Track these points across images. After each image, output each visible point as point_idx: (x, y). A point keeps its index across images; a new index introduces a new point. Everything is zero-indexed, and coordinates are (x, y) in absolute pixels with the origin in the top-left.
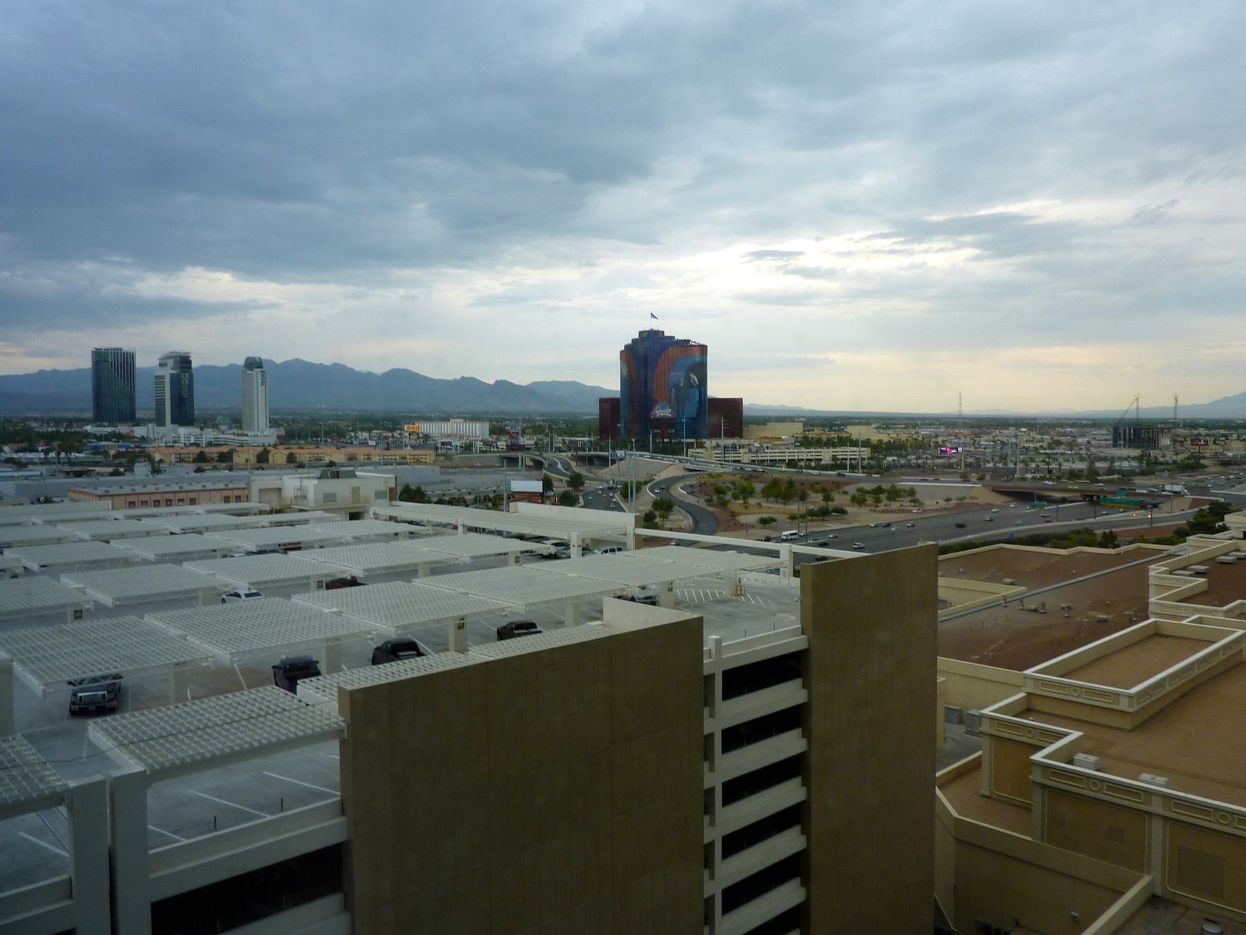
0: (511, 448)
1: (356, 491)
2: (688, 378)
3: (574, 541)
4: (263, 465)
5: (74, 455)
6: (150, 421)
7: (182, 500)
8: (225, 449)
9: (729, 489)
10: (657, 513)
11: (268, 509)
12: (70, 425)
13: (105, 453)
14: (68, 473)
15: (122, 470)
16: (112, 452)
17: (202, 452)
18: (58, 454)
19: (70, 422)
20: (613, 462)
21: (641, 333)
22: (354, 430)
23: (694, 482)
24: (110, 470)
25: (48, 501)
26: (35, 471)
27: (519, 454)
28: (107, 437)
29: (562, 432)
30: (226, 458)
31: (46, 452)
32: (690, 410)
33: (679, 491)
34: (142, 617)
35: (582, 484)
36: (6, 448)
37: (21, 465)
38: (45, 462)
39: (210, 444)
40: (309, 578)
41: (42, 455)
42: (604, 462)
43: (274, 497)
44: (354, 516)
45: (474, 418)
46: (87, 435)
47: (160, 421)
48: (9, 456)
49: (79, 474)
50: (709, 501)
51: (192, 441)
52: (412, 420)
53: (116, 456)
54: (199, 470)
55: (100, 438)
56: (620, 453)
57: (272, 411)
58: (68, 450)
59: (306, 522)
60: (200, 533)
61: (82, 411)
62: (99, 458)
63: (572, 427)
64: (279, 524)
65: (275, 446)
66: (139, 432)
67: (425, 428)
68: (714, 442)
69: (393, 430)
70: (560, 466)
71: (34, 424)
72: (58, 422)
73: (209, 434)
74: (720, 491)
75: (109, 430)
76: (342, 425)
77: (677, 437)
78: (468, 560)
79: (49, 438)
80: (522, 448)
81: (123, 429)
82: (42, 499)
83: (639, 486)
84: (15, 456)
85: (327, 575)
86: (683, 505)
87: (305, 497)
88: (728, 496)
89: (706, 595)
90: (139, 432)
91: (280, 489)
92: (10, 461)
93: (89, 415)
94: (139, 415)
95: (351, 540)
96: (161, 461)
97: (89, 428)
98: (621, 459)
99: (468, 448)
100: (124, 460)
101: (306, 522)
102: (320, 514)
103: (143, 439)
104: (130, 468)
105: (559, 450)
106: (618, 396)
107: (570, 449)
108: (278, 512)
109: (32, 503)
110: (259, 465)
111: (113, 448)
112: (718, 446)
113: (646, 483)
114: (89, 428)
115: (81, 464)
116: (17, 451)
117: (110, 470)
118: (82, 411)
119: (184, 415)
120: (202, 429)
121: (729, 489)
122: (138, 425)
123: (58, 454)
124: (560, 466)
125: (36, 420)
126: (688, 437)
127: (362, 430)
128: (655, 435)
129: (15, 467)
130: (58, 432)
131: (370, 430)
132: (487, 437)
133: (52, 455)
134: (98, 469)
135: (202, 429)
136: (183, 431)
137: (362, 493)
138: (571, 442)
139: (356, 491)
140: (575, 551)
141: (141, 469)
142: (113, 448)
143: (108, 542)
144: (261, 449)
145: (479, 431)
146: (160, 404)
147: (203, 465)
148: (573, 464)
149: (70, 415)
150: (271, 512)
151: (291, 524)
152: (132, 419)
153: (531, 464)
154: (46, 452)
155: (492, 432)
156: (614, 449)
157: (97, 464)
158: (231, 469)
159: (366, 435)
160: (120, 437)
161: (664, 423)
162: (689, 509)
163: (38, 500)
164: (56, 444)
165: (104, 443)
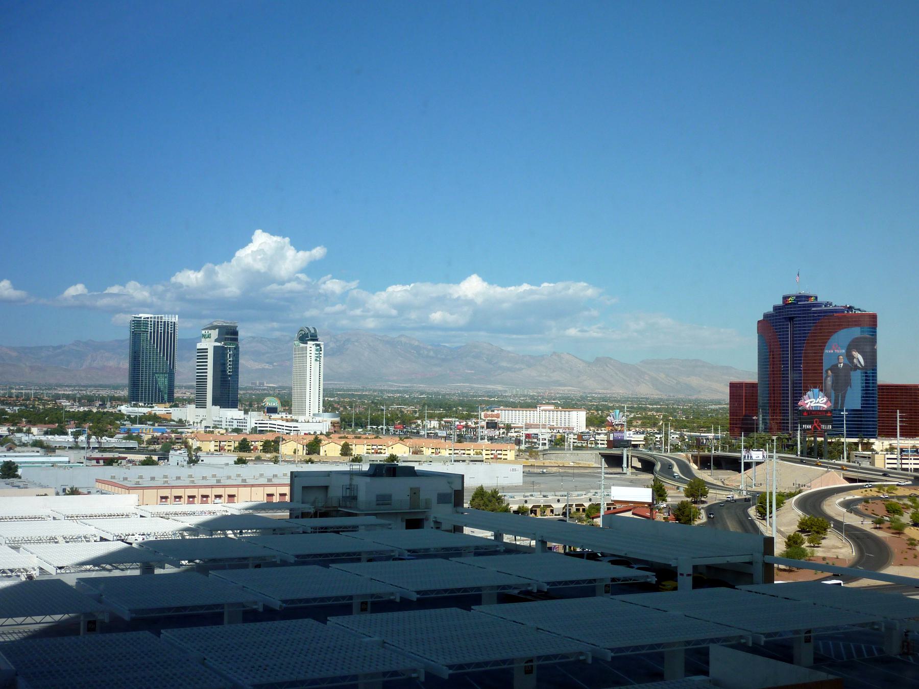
0: (612, 444)
1: (415, 492)
2: (850, 357)
3: (685, 568)
4: (314, 457)
5: (105, 439)
6: (190, 401)
7: (220, 496)
8: (271, 437)
9: (907, 507)
10: (804, 536)
11: (312, 511)
12: (103, 405)
13: (138, 439)
14: (98, 460)
15: (155, 458)
16: (146, 437)
17: (245, 440)
18: (89, 438)
19: (103, 401)
20: (748, 466)
21: (785, 298)
22: (421, 417)
23: (857, 495)
24: (142, 457)
25: (74, 492)
26: (61, 458)
27: (625, 452)
28: (142, 420)
29: (679, 426)
30: (271, 446)
31: (76, 435)
32: (854, 400)
33: (833, 507)
34: (158, 634)
35: (705, 494)
36: (34, 430)
37: (49, 449)
38: (76, 447)
39: (254, 431)
40: (351, 598)
41: (70, 438)
42: (734, 465)
43: (320, 496)
44: (414, 523)
45: (568, 404)
46: (120, 416)
47: (201, 404)
48: (37, 438)
49: (109, 462)
50: (879, 523)
51: (235, 426)
52: (491, 406)
53: (150, 442)
54: (241, 461)
55: (133, 421)
56: (756, 455)
57: (327, 392)
58: (100, 432)
59: (354, 528)
60: (338, 532)
61: (116, 388)
62: (132, 444)
63: (695, 417)
64: (324, 530)
65: (328, 435)
66: (177, 414)
67: (505, 416)
68: (887, 443)
69: (468, 417)
70: (676, 469)
71: (65, 403)
72: (90, 400)
73: (253, 419)
74: (893, 510)
75: (146, 410)
76: (407, 409)
77: (832, 435)
78: (415, 597)
79: (81, 419)
80: (627, 444)
81: (159, 410)
82: (68, 489)
83: (782, 498)
84: (43, 438)
85: (372, 596)
86: (840, 526)
87: (355, 498)
88: (906, 518)
89: (858, 650)
90: (177, 414)
91: (326, 488)
92: (37, 444)
93: (125, 393)
94: (177, 394)
95: (278, 562)
96: (199, 449)
97: (124, 409)
98: (758, 463)
99: (558, 443)
100: (158, 447)
101: (354, 528)
102: (372, 520)
103: (181, 423)
104: (164, 457)
105: (676, 449)
106: (754, 379)
107: (690, 447)
108: (324, 515)
109: (57, 494)
110: (308, 457)
111: (147, 432)
112: (891, 449)
113: (791, 495)
114: (124, 409)
115: (111, 450)
116: (46, 433)
117: (142, 457)
118: (116, 388)
119: (227, 395)
120: (246, 412)
121: (907, 507)
122: (176, 406)
123: (89, 438)
124: (676, 469)
125: (68, 397)
126: (849, 436)
127: (431, 417)
128: (804, 431)
129: (42, 451)
130: (91, 411)
131: (440, 417)
132: (583, 429)
133: (82, 438)
134: (130, 457)
135: (246, 412)
136: (234, 414)
137: (423, 496)
138: (691, 437)
139: (415, 492)
140: (685, 582)
141: (177, 456)
142: (147, 432)
143: (16, 548)
144: (312, 438)
145: (578, 420)
146: (202, 381)
147: (243, 455)
148: (694, 467)
149: (103, 393)
150: (315, 515)
151: (337, 530)
152: (174, 402)
153: (639, 465)
154: (76, 435)
155: (590, 422)
156: (748, 448)
157: (130, 450)
158: (276, 461)
159: (435, 423)
160: (155, 419)
161: (814, 415)
162: (853, 534)
163: (64, 490)
164: (87, 425)
165: (138, 426)
